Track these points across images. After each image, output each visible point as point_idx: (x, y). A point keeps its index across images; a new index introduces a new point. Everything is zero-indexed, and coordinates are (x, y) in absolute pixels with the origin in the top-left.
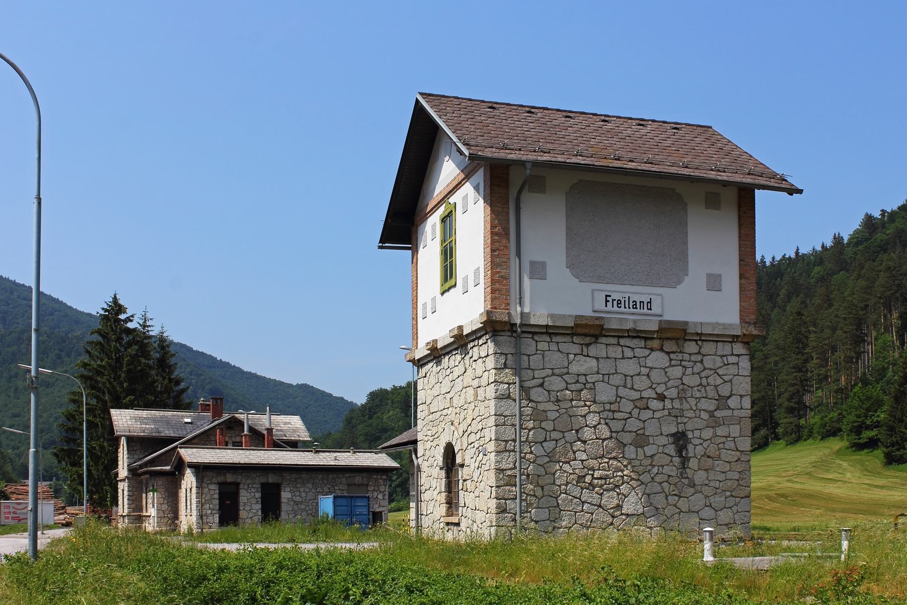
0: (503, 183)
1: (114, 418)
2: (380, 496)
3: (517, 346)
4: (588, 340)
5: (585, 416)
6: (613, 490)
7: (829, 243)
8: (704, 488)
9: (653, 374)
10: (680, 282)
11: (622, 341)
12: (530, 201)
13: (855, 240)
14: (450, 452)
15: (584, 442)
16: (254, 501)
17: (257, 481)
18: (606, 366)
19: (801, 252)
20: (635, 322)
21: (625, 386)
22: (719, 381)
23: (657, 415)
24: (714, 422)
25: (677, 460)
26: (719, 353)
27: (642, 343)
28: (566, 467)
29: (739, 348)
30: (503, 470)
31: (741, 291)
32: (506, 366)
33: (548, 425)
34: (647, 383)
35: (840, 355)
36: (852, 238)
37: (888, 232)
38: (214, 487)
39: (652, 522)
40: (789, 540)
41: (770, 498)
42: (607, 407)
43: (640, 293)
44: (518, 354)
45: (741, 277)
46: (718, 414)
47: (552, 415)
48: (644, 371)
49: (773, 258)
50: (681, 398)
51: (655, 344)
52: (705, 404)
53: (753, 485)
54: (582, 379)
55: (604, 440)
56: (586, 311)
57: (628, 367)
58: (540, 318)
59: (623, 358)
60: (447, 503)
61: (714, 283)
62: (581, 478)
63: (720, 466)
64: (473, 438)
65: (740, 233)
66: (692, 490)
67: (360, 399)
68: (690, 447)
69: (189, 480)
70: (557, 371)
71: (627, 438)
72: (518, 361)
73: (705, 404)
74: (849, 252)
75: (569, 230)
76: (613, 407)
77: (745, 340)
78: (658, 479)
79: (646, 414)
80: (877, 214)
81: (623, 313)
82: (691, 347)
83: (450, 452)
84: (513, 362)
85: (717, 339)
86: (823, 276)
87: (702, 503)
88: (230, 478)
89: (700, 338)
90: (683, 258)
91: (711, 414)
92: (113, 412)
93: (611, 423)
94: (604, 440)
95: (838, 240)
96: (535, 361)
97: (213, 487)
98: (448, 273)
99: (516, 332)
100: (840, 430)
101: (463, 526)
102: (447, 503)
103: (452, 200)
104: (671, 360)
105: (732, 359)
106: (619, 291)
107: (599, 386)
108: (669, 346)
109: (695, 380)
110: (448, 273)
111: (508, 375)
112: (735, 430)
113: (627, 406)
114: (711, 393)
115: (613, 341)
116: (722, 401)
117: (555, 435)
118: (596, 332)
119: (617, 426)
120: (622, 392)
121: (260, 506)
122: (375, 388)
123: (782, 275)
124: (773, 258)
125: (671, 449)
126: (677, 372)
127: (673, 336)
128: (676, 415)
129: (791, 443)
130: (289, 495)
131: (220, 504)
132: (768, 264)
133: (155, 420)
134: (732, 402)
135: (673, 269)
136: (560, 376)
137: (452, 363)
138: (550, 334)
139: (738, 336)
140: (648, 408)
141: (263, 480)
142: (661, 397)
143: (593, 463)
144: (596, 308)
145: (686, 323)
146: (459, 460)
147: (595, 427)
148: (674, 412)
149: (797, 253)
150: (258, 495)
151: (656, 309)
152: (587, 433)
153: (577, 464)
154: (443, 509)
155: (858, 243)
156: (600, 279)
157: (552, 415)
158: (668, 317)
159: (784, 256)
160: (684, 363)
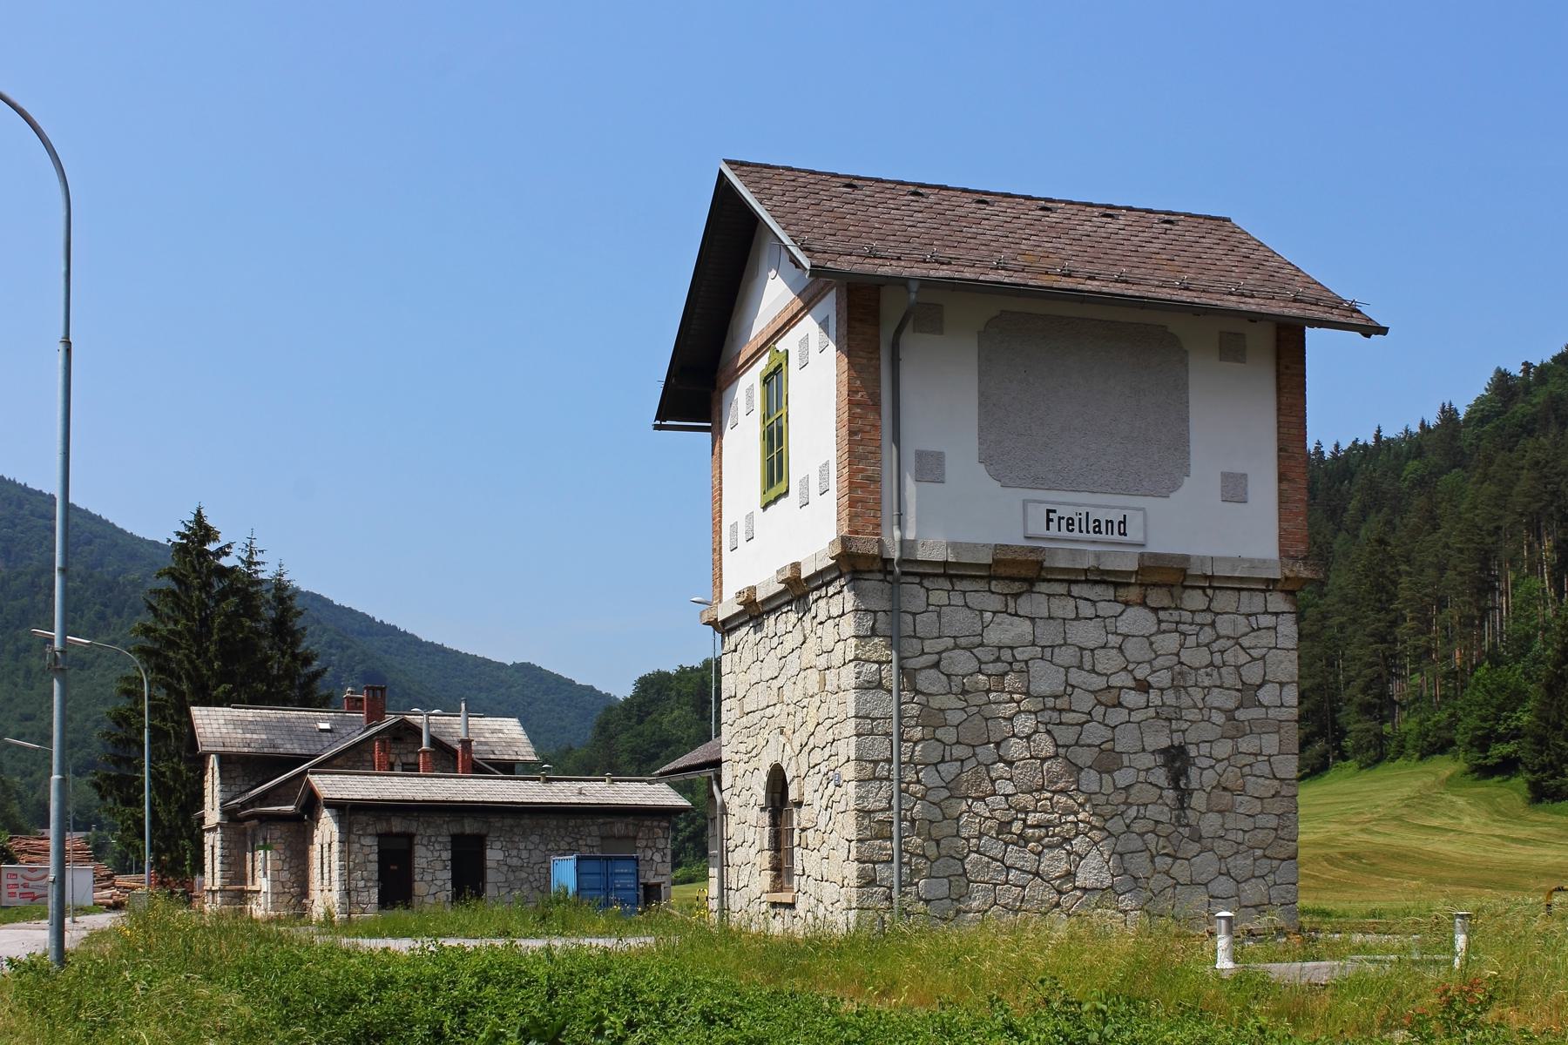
0: (870, 316)
1: (197, 722)
2: (657, 857)
3: (894, 597)
4: (1016, 587)
5: (1011, 719)
6: (1060, 846)
7: (1433, 420)
8: (1218, 843)
9: (1130, 646)
10: (1175, 486)
11: (1076, 590)
12: (916, 347)
13: (1478, 415)
14: (777, 781)
15: (1010, 764)
16: (439, 865)
17: (444, 831)
18: (1048, 633)
19: (1385, 434)
20: (1098, 555)
21: (1080, 667)
22: (1243, 658)
23: (1136, 716)
24: (1235, 729)
25: (1170, 795)
26: (1243, 610)
27: (1110, 593)
28: (979, 807)
29: (1277, 602)
30: (869, 812)
31: (1280, 502)
32: (874, 632)
33: (948, 735)
34: (1119, 661)
35: (1452, 614)
36: (1473, 410)
37: (1535, 401)
38: (370, 842)
39: (1127, 902)
40: (1364, 933)
41: (1330, 860)
42: (1050, 702)
43: (1106, 506)
44: (895, 612)
45: (1282, 478)
46: (1241, 715)
47: (955, 717)
48: (1114, 640)
49: (1337, 446)
50: (1177, 687)
51: (1133, 594)
52: (1218, 699)
53: (1301, 838)
54: (1006, 655)
55: (1044, 760)
56: (1014, 537)
57: (1087, 634)
58: (933, 550)
59: (1077, 618)
60: (773, 869)
61: (1234, 489)
62: (1004, 826)
63: (1245, 804)
64: (817, 756)
65: (1279, 402)
66: (1196, 847)
67: (623, 690)
68: (1193, 772)
69: (327, 828)
70: (963, 642)
71: (1084, 757)
72: (896, 624)
73: (1218, 699)
74: (1468, 436)
75: (983, 397)
76: (1060, 703)
77: (1288, 587)
78: (1137, 827)
79: (1117, 716)
80: (1516, 370)
81: (1077, 541)
82: (1195, 600)
83: (777, 781)
84: (887, 625)
85: (1240, 585)
86: (1423, 477)
87: (1213, 869)
88: (397, 825)
89: (1211, 584)
90: (1181, 446)
91: (1230, 715)
92: (196, 711)
93: (1056, 731)
94: (1044, 760)
95: (1448, 414)
96: (926, 623)
97: (368, 841)
98: (775, 471)
99: (891, 573)
100: (1452, 743)
101: (801, 908)
102: (773, 869)
103: (781, 345)
104: (1160, 622)
105: (1266, 621)
106: (1070, 503)
107: (1036, 666)
108: (1157, 597)
109: (1202, 657)
110: (775, 471)
111: (878, 648)
112: (1270, 743)
113: (1084, 702)
114: (1230, 679)
115: (1061, 589)
116: (1248, 693)
117: (959, 751)
118: (1031, 574)
119: (1066, 735)
120: (1076, 677)
121: (449, 875)
122: (648, 669)
123: (1353, 475)
124: (1337, 446)
125: (1160, 776)
126: (1170, 642)
127: (1164, 580)
128: (1168, 716)
129: (1368, 766)
130: (499, 855)
131: (380, 871)
132: (1327, 455)
133: (267, 726)
134: (1266, 695)
135: (1164, 465)
136: (969, 649)
137: (781, 628)
138: (951, 577)
139: (1275, 581)
140: (1120, 705)
141: (455, 829)
142: (1143, 687)
143: (1026, 800)
144: (1030, 533)
145: (1186, 558)
146: (793, 795)
147: (1028, 737)
148: (1165, 712)
149: (1378, 437)
150: (447, 855)
151: (1134, 534)
152: (1016, 749)
153: (997, 801)
154: (766, 880)
155: (1484, 420)
156: (1037, 482)
157: (955, 717)
158: (1154, 547)
159: (1355, 443)
160: (1182, 627)
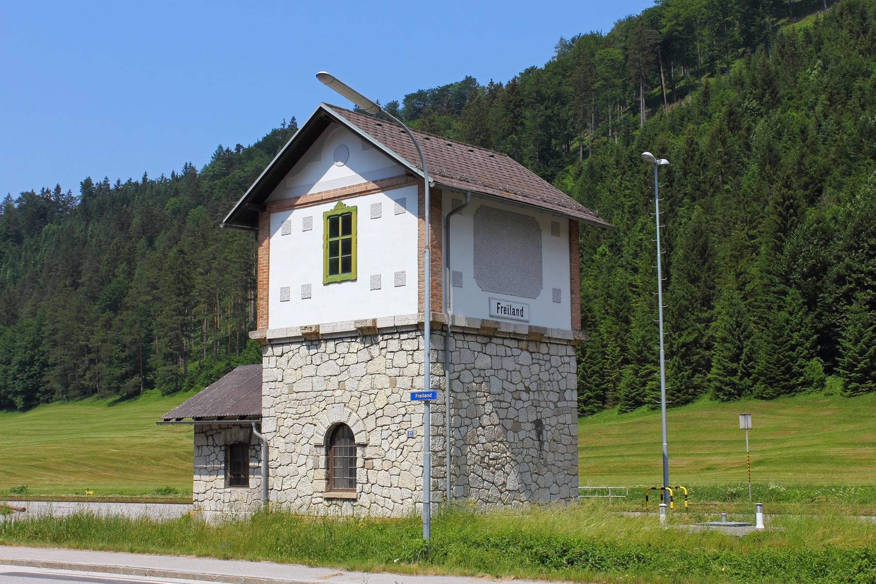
4: (486, 340)
5: (483, 405)
6: (500, 469)
7: (179, 172)
8: (553, 467)
10: (538, 294)
11: (507, 342)
12: (454, 219)
13: (211, 173)
15: (484, 427)
20: (515, 326)
21: (507, 380)
25: (537, 443)
26: (560, 354)
28: (474, 449)
30: (436, 452)
31: (572, 304)
33: (463, 413)
35: (229, 301)
37: (246, 169)
39: (523, 497)
41: (180, 456)
42: (497, 397)
43: (516, 302)
45: (572, 293)
46: (560, 404)
49: (119, 182)
51: (523, 345)
53: (579, 465)
55: (495, 426)
57: (509, 364)
58: (461, 322)
59: (506, 356)
60: (327, 479)
65: (571, 257)
68: (544, 432)
70: (468, 366)
72: (446, 357)
74: (205, 185)
76: (501, 398)
78: (527, 460)
79: (519, 404)
81: (507, 318)
82: (544, 348)
84: (444, 358)
85: (558, 342)
86: (179, 209)
90: (539, 275)
94: (495, 426)
95: (189, 170)
99: (446, 331)
102: (327, 479)
103: (349, 203)
104: (533, 359)
106: (507, 300)
107: (492, 378)
108: (532, 347)
111: (438, 369)
113: (508, 397)
115: (500, 341)
117: (467, 421)
118: (491, 334)
119: (503, 414)
123: (129, 201)
124: (119, 182)
125: (533, 435)
126: (535, 368)
129: (168, 393)
132: (112, 187)
136: (470, 370)
138: (463, 334)
139: (570, 341)
140: (520, 399)
144: (492, 314)
145: (546, 329)
147: (490, 414)
149: (145, 179)
151: (525, 318)
152: (485, 421)
155: (215, 177)
156: (493, 289)
158: (533, 323)
159: (129, 181)
160: (540, 362)
